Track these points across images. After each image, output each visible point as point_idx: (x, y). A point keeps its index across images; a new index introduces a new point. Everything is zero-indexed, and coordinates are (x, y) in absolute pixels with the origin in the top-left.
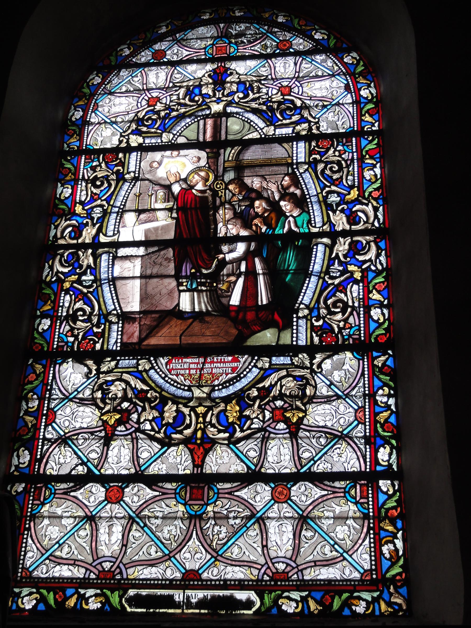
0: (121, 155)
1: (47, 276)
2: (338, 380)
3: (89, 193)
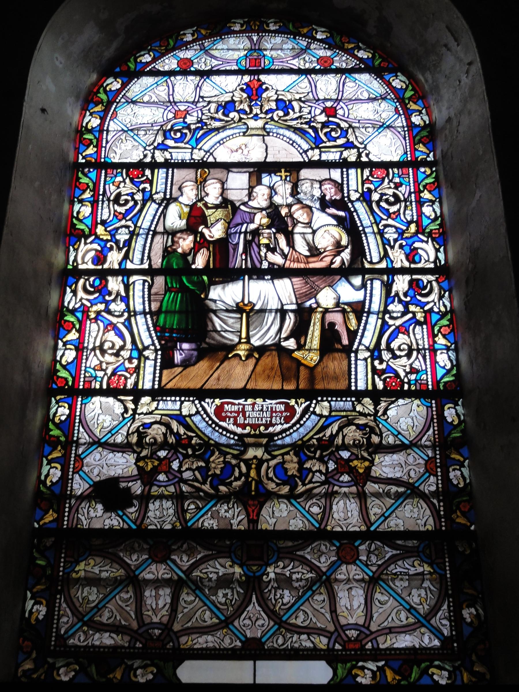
0: (148, 172)
2: (405, 428)
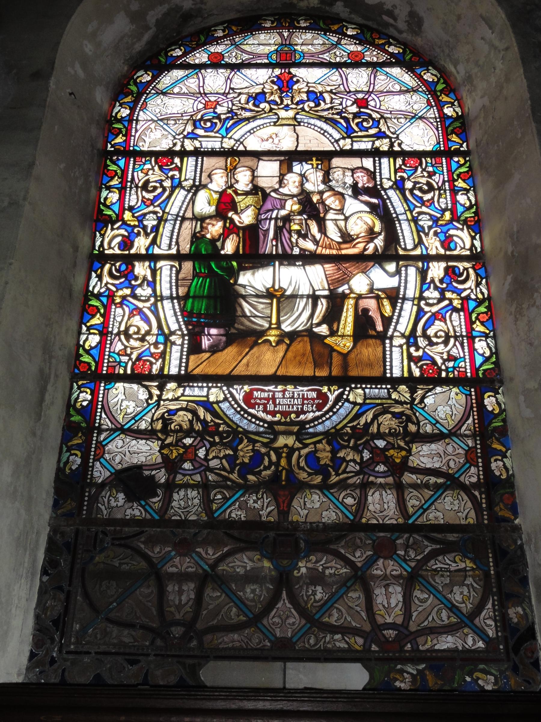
0: (177, 160)
1: (94, 287)
3: (140, 198)
